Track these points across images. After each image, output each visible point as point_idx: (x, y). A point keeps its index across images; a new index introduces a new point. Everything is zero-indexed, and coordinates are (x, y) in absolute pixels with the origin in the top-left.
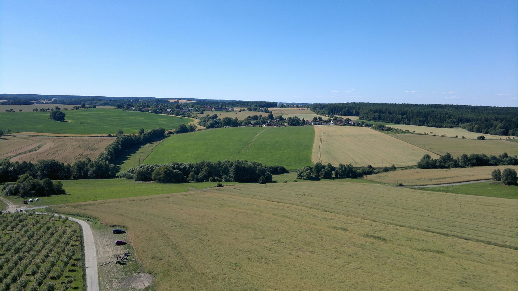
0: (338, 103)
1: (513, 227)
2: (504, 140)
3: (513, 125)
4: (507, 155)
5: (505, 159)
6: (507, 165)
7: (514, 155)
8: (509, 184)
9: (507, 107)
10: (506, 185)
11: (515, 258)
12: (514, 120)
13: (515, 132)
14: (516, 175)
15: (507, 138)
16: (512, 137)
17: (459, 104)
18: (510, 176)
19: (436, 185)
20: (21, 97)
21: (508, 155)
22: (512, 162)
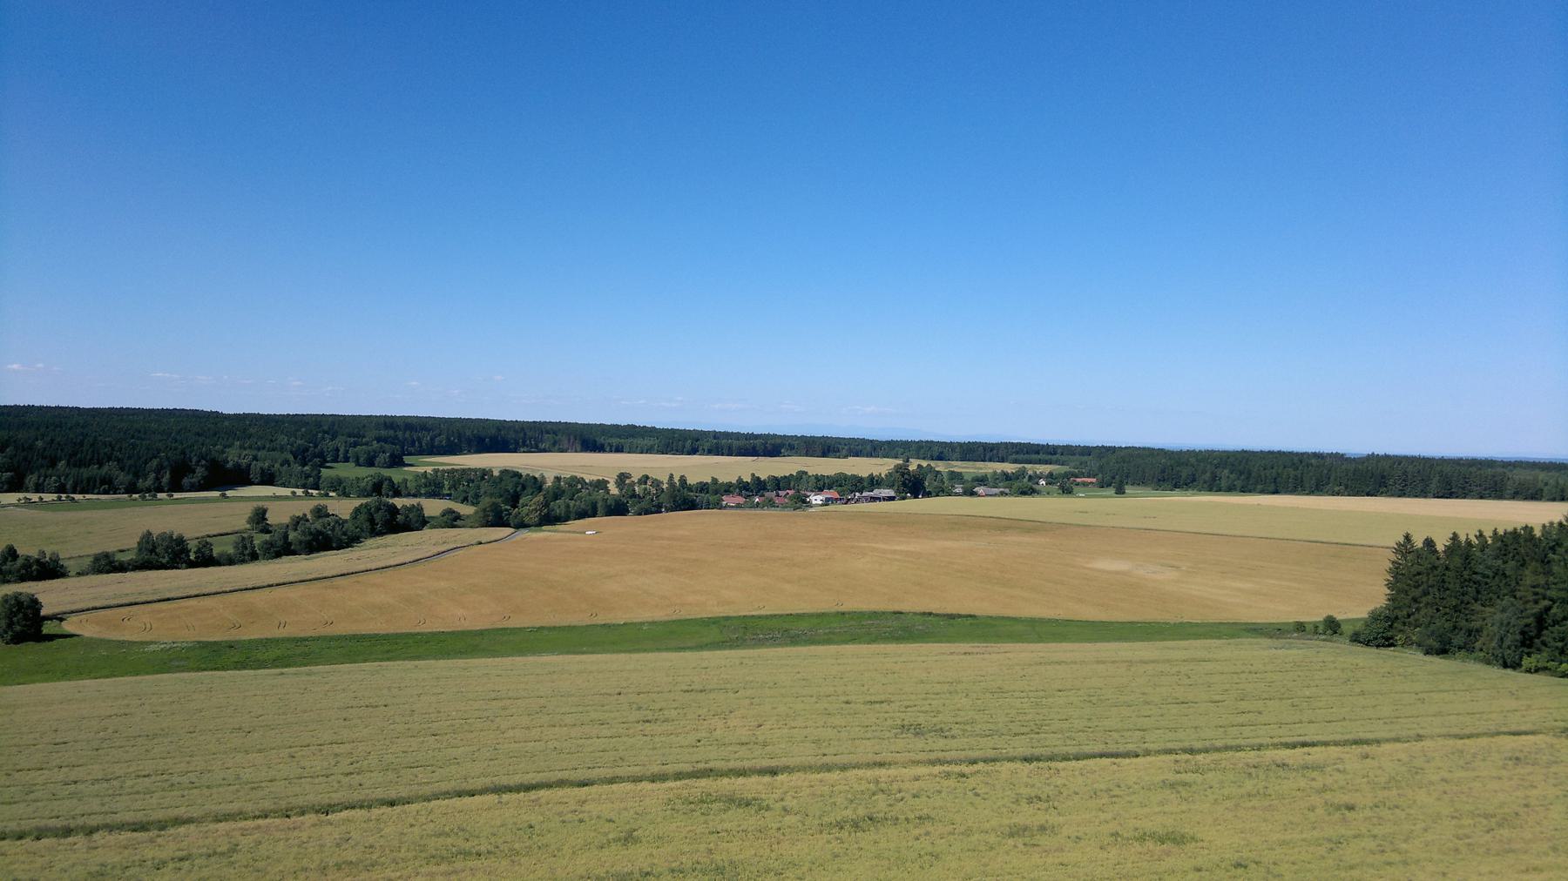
0: (532, 420)
1: (18, 771)
2: (10, 505)
3: (38, 459)
4: (15, 551)
5: (9, 563)
6: (15, 582)
7: (37, 551)
8: (18, 639)
9: (22, 405)
10: (7, 643)
11: (16, 866)
12: (39, 443)
13: (45, 481)
14: (39, 610)
15: (19, 500)
16: (35, 497)
17: (1380, 451)
18: (21, 615)
19: (568, 534)
20: (409, 420)
21: (18, 552)
22: (32, 572)
